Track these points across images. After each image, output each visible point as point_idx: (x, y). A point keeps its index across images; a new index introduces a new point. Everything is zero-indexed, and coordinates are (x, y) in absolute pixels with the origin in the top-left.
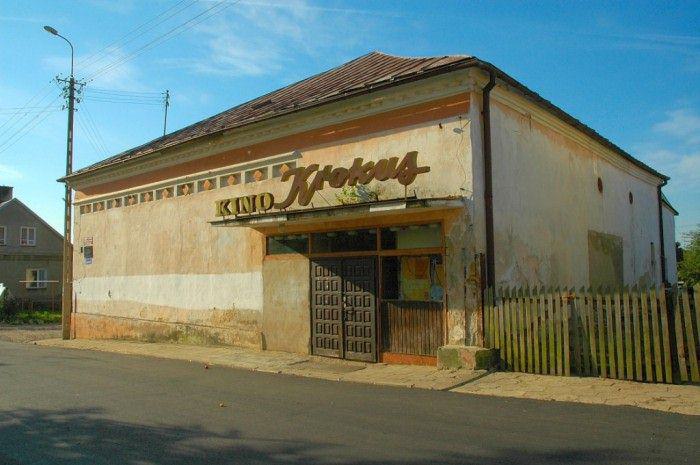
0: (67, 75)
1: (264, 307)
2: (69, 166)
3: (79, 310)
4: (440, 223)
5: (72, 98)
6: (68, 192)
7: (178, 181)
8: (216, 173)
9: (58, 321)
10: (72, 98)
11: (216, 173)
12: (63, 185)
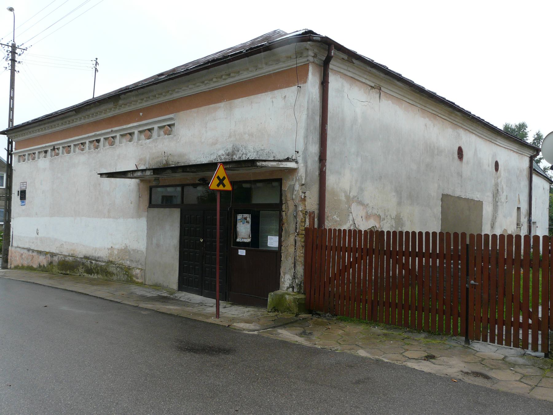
0: (8, 40)
1: (147, 249)
2: (11, 120)
3: (15, 244)
4: (280, 181)
5: (13, 61)
6: (10, 143)
7: (89, 137)
8: (116, 131)
9: (25, 205)
10: (13, 61)
11: (116, 131)
12: (5, 138)
